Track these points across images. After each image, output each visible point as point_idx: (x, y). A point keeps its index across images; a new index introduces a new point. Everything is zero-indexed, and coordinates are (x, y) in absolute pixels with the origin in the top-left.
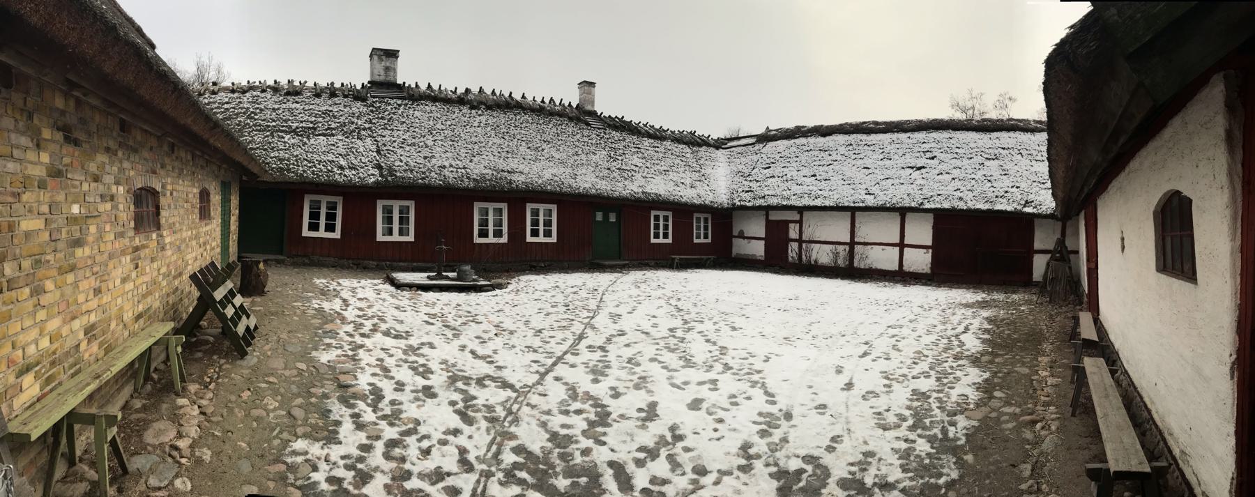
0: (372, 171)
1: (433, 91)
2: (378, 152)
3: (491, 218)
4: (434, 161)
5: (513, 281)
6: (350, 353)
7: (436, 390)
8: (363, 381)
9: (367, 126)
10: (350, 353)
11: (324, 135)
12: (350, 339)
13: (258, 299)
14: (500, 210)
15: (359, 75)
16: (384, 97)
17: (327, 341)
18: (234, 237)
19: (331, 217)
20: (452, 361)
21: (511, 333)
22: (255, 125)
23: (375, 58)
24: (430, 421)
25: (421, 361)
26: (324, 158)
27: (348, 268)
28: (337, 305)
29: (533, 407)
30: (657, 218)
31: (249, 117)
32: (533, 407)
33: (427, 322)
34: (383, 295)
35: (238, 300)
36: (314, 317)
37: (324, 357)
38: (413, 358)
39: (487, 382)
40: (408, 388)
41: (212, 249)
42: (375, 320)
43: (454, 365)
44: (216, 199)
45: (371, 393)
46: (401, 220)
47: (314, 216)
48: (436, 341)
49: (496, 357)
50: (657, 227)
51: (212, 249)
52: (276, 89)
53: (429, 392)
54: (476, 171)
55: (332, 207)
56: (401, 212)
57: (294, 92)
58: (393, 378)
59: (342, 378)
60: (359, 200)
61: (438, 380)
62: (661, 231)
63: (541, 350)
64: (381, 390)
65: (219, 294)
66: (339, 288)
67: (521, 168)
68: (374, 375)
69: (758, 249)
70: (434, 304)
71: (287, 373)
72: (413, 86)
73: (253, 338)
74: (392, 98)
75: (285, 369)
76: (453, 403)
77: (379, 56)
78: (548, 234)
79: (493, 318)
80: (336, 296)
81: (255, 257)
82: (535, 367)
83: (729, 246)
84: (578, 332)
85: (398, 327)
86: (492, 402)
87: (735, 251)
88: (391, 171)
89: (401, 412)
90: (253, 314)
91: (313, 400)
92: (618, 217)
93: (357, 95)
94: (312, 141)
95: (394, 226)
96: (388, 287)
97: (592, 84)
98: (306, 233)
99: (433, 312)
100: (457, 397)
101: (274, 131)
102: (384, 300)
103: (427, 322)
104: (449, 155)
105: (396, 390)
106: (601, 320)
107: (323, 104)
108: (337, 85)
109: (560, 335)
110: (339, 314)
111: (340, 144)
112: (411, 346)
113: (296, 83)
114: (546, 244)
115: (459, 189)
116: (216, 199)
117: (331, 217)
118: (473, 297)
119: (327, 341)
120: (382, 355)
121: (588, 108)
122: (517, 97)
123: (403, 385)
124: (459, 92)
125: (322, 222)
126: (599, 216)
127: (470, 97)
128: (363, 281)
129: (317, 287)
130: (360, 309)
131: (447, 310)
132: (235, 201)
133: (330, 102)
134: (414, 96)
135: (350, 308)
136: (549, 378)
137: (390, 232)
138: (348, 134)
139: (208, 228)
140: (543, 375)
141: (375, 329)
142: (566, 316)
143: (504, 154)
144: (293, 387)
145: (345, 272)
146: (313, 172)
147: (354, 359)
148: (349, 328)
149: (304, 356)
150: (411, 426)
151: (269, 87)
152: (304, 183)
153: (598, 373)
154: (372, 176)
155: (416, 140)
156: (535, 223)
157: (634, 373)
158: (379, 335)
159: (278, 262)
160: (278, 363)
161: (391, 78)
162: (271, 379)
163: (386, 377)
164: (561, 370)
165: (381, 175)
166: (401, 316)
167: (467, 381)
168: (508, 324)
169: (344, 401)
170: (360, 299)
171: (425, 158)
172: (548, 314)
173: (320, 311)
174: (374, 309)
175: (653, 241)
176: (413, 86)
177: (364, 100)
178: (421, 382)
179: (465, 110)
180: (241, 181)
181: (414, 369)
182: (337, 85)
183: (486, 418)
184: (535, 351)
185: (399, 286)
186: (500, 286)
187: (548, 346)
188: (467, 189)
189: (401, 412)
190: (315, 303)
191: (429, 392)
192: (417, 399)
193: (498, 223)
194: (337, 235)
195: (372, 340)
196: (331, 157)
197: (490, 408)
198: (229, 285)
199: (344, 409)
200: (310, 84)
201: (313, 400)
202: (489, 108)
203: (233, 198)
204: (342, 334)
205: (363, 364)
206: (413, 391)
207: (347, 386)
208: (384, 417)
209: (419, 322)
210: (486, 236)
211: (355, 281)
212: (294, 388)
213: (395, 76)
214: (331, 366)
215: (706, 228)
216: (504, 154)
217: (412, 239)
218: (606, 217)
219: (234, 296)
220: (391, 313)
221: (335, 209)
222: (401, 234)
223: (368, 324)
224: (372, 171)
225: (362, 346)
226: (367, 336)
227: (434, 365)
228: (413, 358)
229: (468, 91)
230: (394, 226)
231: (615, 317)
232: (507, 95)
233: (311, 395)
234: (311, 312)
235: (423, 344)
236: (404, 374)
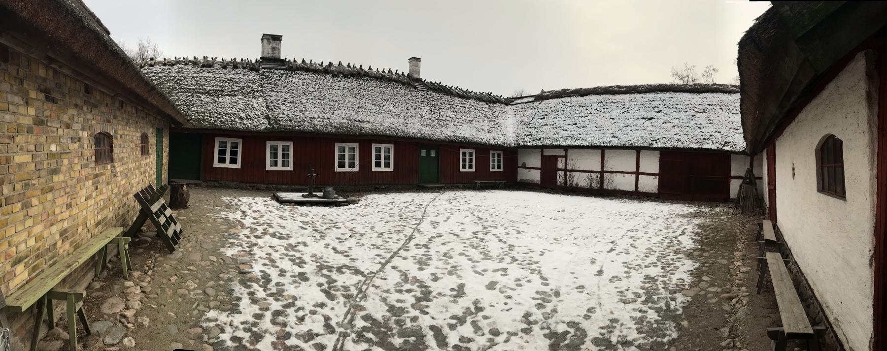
0: (263, 121)
1: (306, 64)
2: (267, 107)
3: (347, 154)
4: (307, 114)
5: (362, 199)
6: (247, 249)
7: (308, 276)
8: (257, 269)
9: (259, 89)
10: (247, 249)
11: (229, 95)
12: (247, 240)
13: (182, 211)
14: (354, 148)
15: (254, 53)
16: (271, 69)
17: (231, 241)
18: (165, 168)
19: (234, 153)
20: (319, 255)
21: (361, 235)
22: (180, 88)
23: (265, 41)
24: (304, 297)
25: (298, 255)
26: (229, 111)
27: (246, 189)
28: (238, 215)
29: (377, 287)
30: (464, 154)
31: (176, 83)
32: (377, 287)
33: (302, 228)
34: (271, 208)
35: (168, 212)
36: (222, 224)
37: (229, 252)
38: (292, 253)
39: (344, 270)
40: (288, 274)
41: (150, 176)
42: (265, 226)
43: (321, 258)
45: (262, 278)
46: (284, 155)
47: (222, 152)
48: (308, 241)
49: (351, 252)
50: (464, 160)
51: (150, 176)
52: (195, 63)
53: (303, 277)
54: (337, 121)
55: (235, 146)
56: (283, 150)
57: (208, 65)
58: (277, 267)
59: (242, 267)
60: (254, 141)
61: (309, 268)
62: (467, 163)
63: (382, 247)
64: (270, 276)
65: (155, 208)
66: (239, 204)
68: (264, 265)
69: (536, 176)
70: (307, 215)
71: (203, 263)
72: (292, 61)
73: (179, 238)
74: (277, 69)
75: (202, 260)
76: (320, 285)
77: (268, 40)
78: (387, 165)
79: (349, 224)
80: (237, 209)
81: (181, 182)
82: (378, 259)
83: (516, 174)
84: (409, 235)
85: (282, 231)
86: (347, 284)
87: (519, 177)
88: (276, 121)
89: (283, 291)
90: (179, 222)
91: (221, 282)
92: (437, 154)
93: (252, 67)
94: (221, 100)
95: (279, 160)
96: (274, 203)
97: (418, 60)
98: (216, 164)
99: (306, 220)
100: (323, 280)
101: (193, 93)
102: (271, 212)
103: (302, 228)
104: (317, 109)
105: (280, 275)
106: (425, 226)
107: (229, 74)
108: (239, 60)
109: (395, 237)
110: (240, 222)
111: (240, 102)
112: (290, 245)
113: (210, 59)
114: (386, 172)
115: (324, 134)
117: (234, 153)
118: (334, 210)
119: (231, 241)
120: (270, 251)
121: (416, 76)
123: (285, 272)
124: (324, 65)
125: (228, 157)
126: (424, 153)
127: (332, 68)
128: (257, 199)
129: (224, 203)
130: (254, 218)
131: (316, 219)
132: (166, 142)
133: (233, 72)
134: (292, 68)
135: (247, 218)
136: (388, 267)
137: (275, 164)
138: (246, 95)
139: (147, 161)
140: (384, 265)
141: (265, 232)
142: (400, 223)
144: (207, 273)
145: (244, 192)
146: (221, 122)
147: (250, 253)
148: (247, 232)
149: (215, 251)
150: (290, 301)
151: (190, 61)
152: (215, 129)
153: (422, 263)
154: (263, 125)
155: (294, 99)
156: (378, 157)
157: (448, 264)
158: (268, 237)
159: (197, 185)
160: (196, 257)
161: (276, 55)
162: (192, 268)
163: (273, 266)
164: (396, 261)
165: (270, 124)
166: (283, 223)
167: (330, 269)
168: (359, 229)
169: (243, 283)
170: (254, 211)
171: (301, 111)
172: (387, 222)
173: (226, 219)
174: (264, 219)
175: (462, 170)
176: (292, 61)
177: (257, 70)
178: (297, 270)
179: (329, 77)
180: (170, 128)
181: (292, 261)
182: (239, 60)
183: (343, 295)
184: (378, 248)
185: (282, 202)
186: (353, 202)
187: (387, 244)
188: (330, 134)
189: (283, 291)
190: (223, 214)
191: (303, 277)
192: (295, 282)
193: (352, 158)
194: (238, 166)
195: (263, 240)
196: (234, 111)
197: (346, 288)
198: (162, 201)
199: (243, 289)
200: (219, 59)
201: (221, 282)
202: (346, 76)
203: (164, 140)
204: (242, 236)
205: (256, 257)
206: (292, 276)
207: (245, 273)
208: (272, 295)
209: (296, 227)
210: (344, 166)
211: (251, 198)
212: (208, 274)
213: (279, 54)
214: (234, 259)
215: (499, 161)
217: (291, 169)
218: (428, 153)
219: (165, 209)
220: (276, 221)
221: (237, 147)
222: (283, 165)
223: (260, 229)
224: (263, 121)
225: (256, 245)
226: (260, 237)
227: (307, 258)
228: (292, 253)
229: (331, 64)
230: (279, 160)
233: (220, 279)
234: (220, 220)
235: (299, 243)
236: (286, 264)
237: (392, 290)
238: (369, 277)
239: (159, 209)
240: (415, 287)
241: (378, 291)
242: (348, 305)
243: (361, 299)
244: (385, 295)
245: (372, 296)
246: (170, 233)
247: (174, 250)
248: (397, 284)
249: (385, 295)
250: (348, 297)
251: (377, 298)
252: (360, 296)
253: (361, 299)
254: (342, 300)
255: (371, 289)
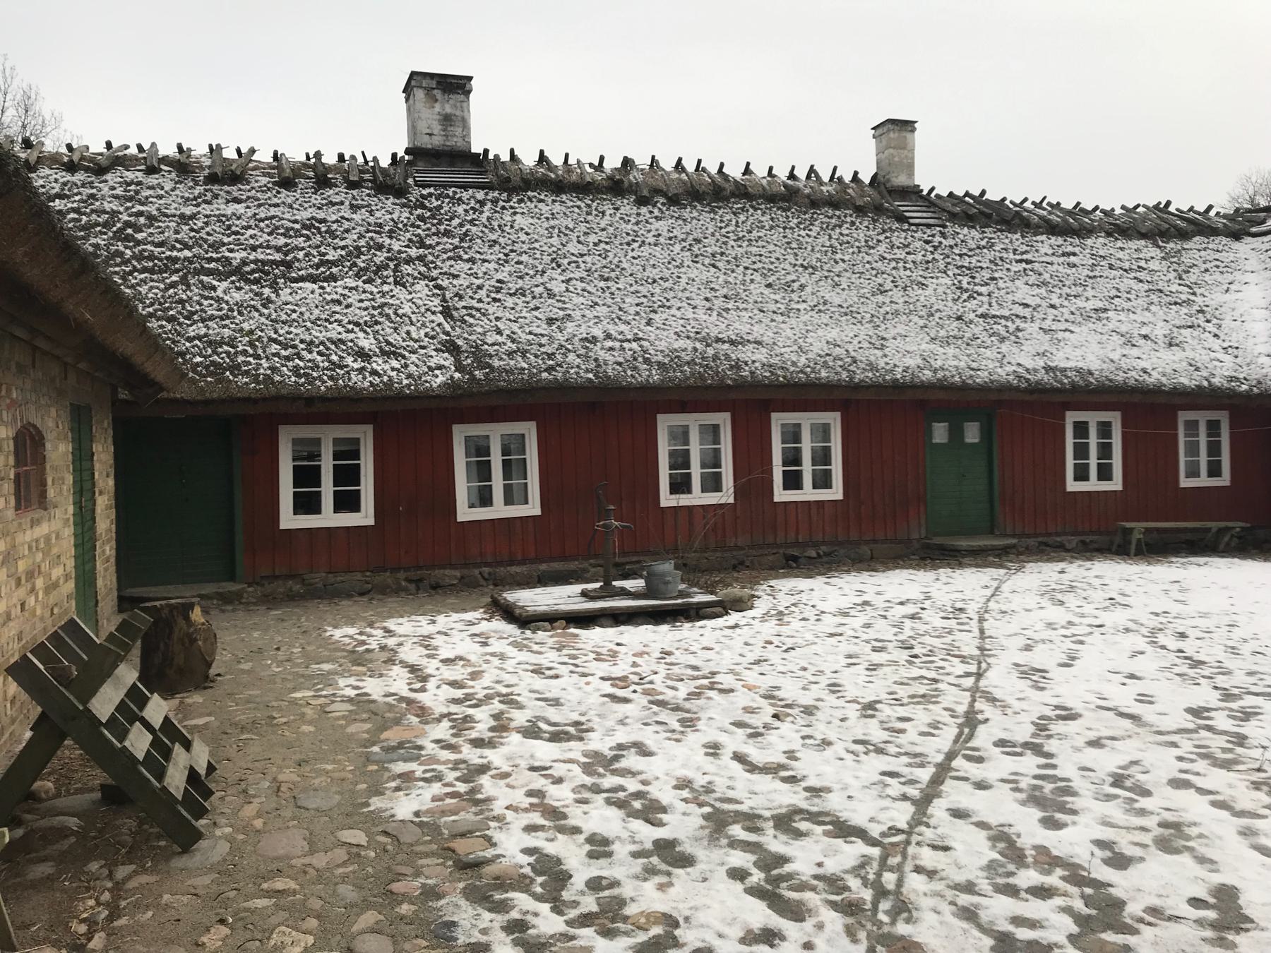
0: (437, 359)
1: (551, 168)
2: (447, 312)
3: (695, 450)
4: (570, 327)
5: (762, 590)
6: (462, 788)
7: (687, 848)
8: (511, 846)
9: (414, 252)
10: (462, 788)
11: (313, 279)
12: (453, 757)
13: (196, 698)
14: (715, 429)
15: (383, 136)
16: (446, 186)
17: (400, 767)
18: (106, 550)
19: (347, 475)
20: (700, 781)
21: (809, 711)
22: (139, 258)
23: (419, 94)
24: (701, 917)
25: (632, 785)
26: (318, 334)
27: (397, 591)
28: (398, 682)
29: (931, 874)
31: (120, 236)
32: (931, 874)
33: (613, 698)
34: (496, 646)
35: (157, 709)
36: (351, 718)
37: (405, 807)
38: (609, 781)
39: (804, 826)
40: (621, 850)
41: (51, 587)
42: (496, 706)
43: (708, 789)
44: (59, 451)
45: (539, 873)
47: (306, 476)
48: (649, 737)
49: (799, 768)
51: (51, 587)
52: (182, 165)
53: (670, 855)
54: (662, 345)
55: (347, 452)
56: (505, 451)
57: (227, 174)
58: (576, 830)
59: (461, 846)
60: (411, 426)
61: (683, 824)
63: (892, 749)
64: (559, 861)
65: (105, 703)
66: (391, 642)
67: (758, 331)
68: (531, 829)
70: (614, 654)
71: (320, 860)
72: (505, 157)
73: (208, 793)
74: (465, 187)
75: (312, 852)
76: (738, 874)
77: (429, 90)
78: (823, 481)
79: (751, 677)
80: (390, 661)
81: (176, 594)
82: (895, 787)
84: (961, 709)
85: (553, 714)
86: (832, 867)
88: (479, 355)
89: (622, 902)
90: (200, 735)
91: (405, 909)
93: (382, 182)
94: (285, 294)
95: (496, 486)
96: (499, 625)
98: (289, 519)
99: (617, 672)
100: (740, 859)
101: (190, 272)
102: (502, 657)
103: (613, 698)
104: (602, 311)
105: (592, 855)
106: (1000, 679)
107: (301, 206)
108: (330, 159)
109: (922, 716)
110: (410, 702)
111: (353, 298)
112: (596, 755)
113: (229, 154)
115: (629, 389)
116: (59, 451)
117: (347, 475)
118: (688, 632)
119: (400, 767)
120: (539, 782)
122: (735, 172)
123: (606, 842)
124: (608, 165)
125: (327, 489)
127: (635, 176)
128: (441, 619)
129: (336, 647)
130: (454, 684)
131: (646, 666)
132: (103, 456)
133: (317, 199)
134: (512, 181)
135: (431, 685)
136: (938, 809)
137: (485, 498)
138: (371, 274)
139: (43, 529)
140: (923, 803)
141: (501, 726)
142: (916, 672)
143: (718, 303)
144: (342, 889)
145: (392, 602)
146: (296, 371)
147: (473, 799)
148: (442, 730)
149: (355, 813)
150: (657, 930)
151: (165, 160)
152: (277, 398)
153: (1053, 802)
154: (439, 372)
155: (526, 283)
156: (793, 458)
157: (1142, 812)
158: (514, 740)
159: (227, 599)
160: (289, 843)
161: (456, 142)
162: (279, 884)
163: (562, 830)
164: (955, 794)
165: (459, 368)
166: (552, 688)
167: (751, 820)
168: (790, 690)
169: (479, 898)
170: (446, 661)
171: (550, 321)
172: (873, 667)
173: (362, 702)
174: (486, 680)
176: (505, 157)
177: (400, 192)
178: (648, 834)
179: (627, 206)
180: (115, 402)
181: (621, 804)
182: (330, 159)
183: (834, 905)
184: (880, 751)
185: (526, 621)
186: (740, 605)
187: (903, 739)
188: (645, 388)
189: (622, 902)
190: (346, 686)
191: (670, 855)
192: (650, 872)
193: (713, 460)
194: (365, 517)
195: (503, 750)
196: (334, 331)
197: (834, 883)
198: (128, 674)
199: (487, 916)
200: (264, 156)
201: (405, 909)
202: (673, 201)
203: (97, 448)
204: (430, 748)
205: (498, 808)
206: (636, 855)
207: (477, 865)
208: (585, 920)
209: (595, 699)
211: (423, 620)
212: (348, 892)
214: (425, 825)
216: (718, 303)
217: (537, 511)
219: (143, 702)
220: (525, 685)
221: (356, 455)
222: (509, 501)
223: (483, 719)
224: (437, 359)
225: (483, 769)
226: (490, 744)
227: (664, 793)
228: (609, 781)
229: (627, 162)
230: (496, 486)
231: (1034, 676)
232: (713, 170)
233: (394, 899)
234: (341, 708)
235: (620, 747)
236: (601, 818)
237: (984, 885)
238: (893, 847)
239: (121, 708)
240: (1054, 879)
241: (938, 886)
242: (862, 935)
243: (895, 914)
244: (965, 899)
245: (926, 903)
246: (176, 780)
247: (198, 835)
248: (991, 867)
249: (965, 899)
250: (850, 908)
251: (947, 909)
252: (885, 905)
253: (895, 914)
254: (834, 921)
255: (915, 883)
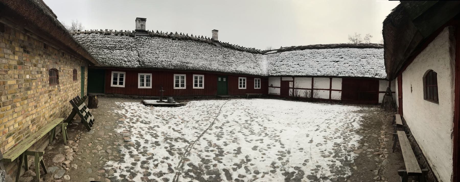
0: (136, 63)
1: (159, 33)
2: (139, 56)
3: (180, 80)
4: (159, 59)
5: (188, 103)
6: (128, 129)
7: (160, 143)
8: (133, 140)
9: (134, 46)
10: (128, 129)
11: (119, 49)
12: (128, 124)
13: (95, 110)
14: (183, 77)
15: (132, 27)
16: (141, 36)
17: (120, 125)
18: (86, 87)
19: (121, 79)
20: (166, 132)
21: (187, 122)
22: (93, 46)
23: (138, 21)
24: (158, 154)
25: (154, 132)
26: (119, 58)
27: (128, 98)
28: (123, 112)
29: (195, 149)
30: (241, 80)
31: (91, 43)
32: (195, 149)
33: (157, 118)
34: (140, 108)
35: (87, 110)
36: (115, 116)
37: (119, 131)
38: (151, 131)
39: (179, 140)
40: (150, 142)
41: (78, 91)
42: (138, 117)
43: (166, 134)
44: (79, 73)
45: (136, 144)
46: (147, 81)
47: (115, 79)
48: (160, 125)
49: (182, 131)
50: (241, 83)
51: (78, 91)
52: (101, 33)
53: (157, 144)
54: (175, 63)
55: (122, 76)
56: (147, 78)
57: (108, 34)
58: (144, 138)
59: (125, 138)
60: (132, 73)
61: (160, 139)
62: (242, 85)
63: (198, 128)
64: (140, 143)
65: (80, 108)
66: (124, 106)
67: (191, 61)
68: (137, 137)
69: (278, 91)
70: (159, 111)
71: (105, 137)
72: (151, 31)
73: (93, 124)
74: (144, 36)
75: (105, 135)
76: (166, 148)
77: (139, 21)
78: (201, 86)
79: (181, 116)
80: (123, 108)
81: (94, 94)
82: (196, 134)
83: (267, 90)
84: (212, 122)
85: (146, 120)
86: (180, 147)
87: (269, 92)
88: (143, 62)
89: (147, 151)
90: (93, 115)
91: (115, 146)
92: (227, 80)
93: (131, 35)
94: (114, 52)
95: (145, 83)
96: (142, 105)
97: (217, 31)
98: (112, 85)
99: (159, 114)
100: (167, 145)
101: (100, 48)
102: (141, 110)
103: (157, 118)
104: (165, 57)
105: (145, 143)
106: (220, 117)
107: (119, 38)
108: (124, 31)
109: (205, 123)
110: (124, 115)
111: (125, 53)
112: (151, 127)
113: (109, 31)
114: (200, 89)
115: (168, 69)
116: (79, 73)
117: (121, 79)
118: (173, 109)
119: (120, 125)
120: (140, 130)
121: (216, 39)
122: (190, 35)
123: (148, 141)
124: (168, 34)
125: (118, 81)
126: (220, 79)
127: (172, 35)
128: (133, 103)
129: (116, 105)
130: (132, 113)
131: (164, 113)
132: (86, 74)
133: (121, 37)
134: (152, 35)
135: (128, 113)
136: (201, 138)
137: (143, 85)
138: (127, 49)
139: (76, 83)
140: (199, 138)
141: (137, 120)
142: (207, 116)
143: (185, 56)
144: (107, 142)
145: (126, 100)
146: (115, 63)
147: (130, 131)
148: (128, 120)
149: (112, 130)
150: (151, 156)
151: (98, 32)
152: (112, 67)
153: (219, 137)
154: (136, 65)
155: (153, 51)
156: (196, 82)
157: (232, 137)
158: (139, 123)
159: (102, 96)
160: (102, 133)
161: (143, 29)
162: (99, 139)
163: (142, 138)
164: (205, 135)
165: (140, 64)
166: (147, 116)
167: (171, 139)
168: (186, 119)
169: (126, 147)
170: (132, 110)
171: (156, 58)
172: (201, 115)
173: (117, 114)
174: (137, 113)
175: (239, 88)
176: (151, 31)
177: (133, 36)
178: (154, 140)
179: (171, 40)
180: (88, 66)
181: (152, 135)
182: (124, 31)
183: (178, 153)
184: (196, 129)
185: (146, 105)
186: (183, 105)
187: (201, 127)
188: (171, 69)
189: (147, 151)
190: (116, 111)
191: (157, 144)
192: (153, 146)
193: (183, 82)
194: (123, 86)
195: (136, 124)
196: (121, 57)
197: (180, 150)
198: (84, 104)
199: (126, 150)
200: (114, 31)
201: (115, 146)
202: (179, 39)
203: (85, 72)
204: (125, 122)
205: (133, 133)
206: (151, 143)
207: (127, 142)
208: (141, 153)
209: (154, 118)
210: (178, 86)
211: (130, 103)
212: (108, 142)
213: (145, 28)
214: (121, 134)
215: (259, 84)
216: (185, 56)
217: (151, 88)
218: (222, 79)
219: (86, 108)
220: (143, 115)
221: (123, 76)
222: (147, 86)
223: (135, 119)
224: (136, 63)
225: (133, 127)
226: (135, 123)
227: (159, 134)
228: (151, 131)
229: (171, 33)
230: (145, 83)
231: (225, 116)
232: (186, 35)
233: (114, 145)
234: (114, 114)
235: (155, 126)
236: (148, 137)
